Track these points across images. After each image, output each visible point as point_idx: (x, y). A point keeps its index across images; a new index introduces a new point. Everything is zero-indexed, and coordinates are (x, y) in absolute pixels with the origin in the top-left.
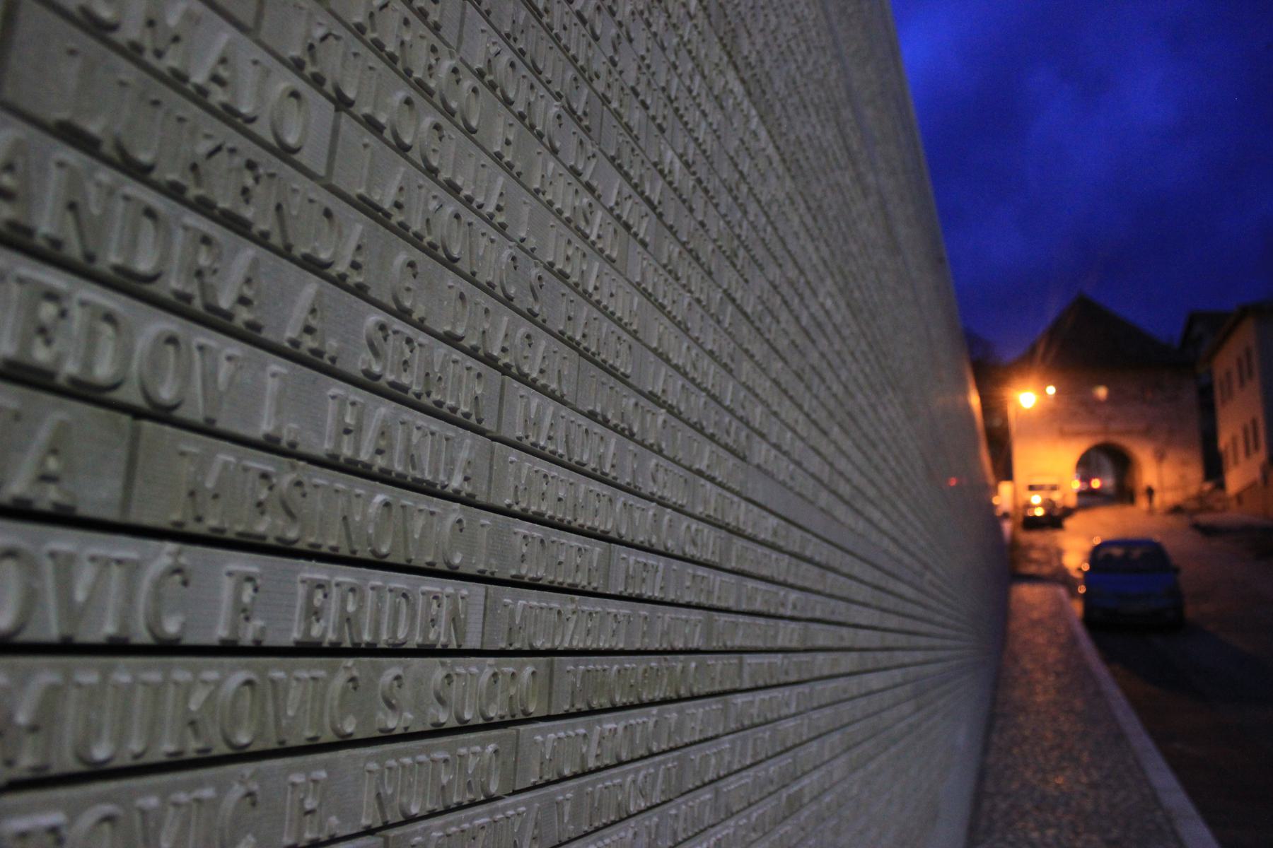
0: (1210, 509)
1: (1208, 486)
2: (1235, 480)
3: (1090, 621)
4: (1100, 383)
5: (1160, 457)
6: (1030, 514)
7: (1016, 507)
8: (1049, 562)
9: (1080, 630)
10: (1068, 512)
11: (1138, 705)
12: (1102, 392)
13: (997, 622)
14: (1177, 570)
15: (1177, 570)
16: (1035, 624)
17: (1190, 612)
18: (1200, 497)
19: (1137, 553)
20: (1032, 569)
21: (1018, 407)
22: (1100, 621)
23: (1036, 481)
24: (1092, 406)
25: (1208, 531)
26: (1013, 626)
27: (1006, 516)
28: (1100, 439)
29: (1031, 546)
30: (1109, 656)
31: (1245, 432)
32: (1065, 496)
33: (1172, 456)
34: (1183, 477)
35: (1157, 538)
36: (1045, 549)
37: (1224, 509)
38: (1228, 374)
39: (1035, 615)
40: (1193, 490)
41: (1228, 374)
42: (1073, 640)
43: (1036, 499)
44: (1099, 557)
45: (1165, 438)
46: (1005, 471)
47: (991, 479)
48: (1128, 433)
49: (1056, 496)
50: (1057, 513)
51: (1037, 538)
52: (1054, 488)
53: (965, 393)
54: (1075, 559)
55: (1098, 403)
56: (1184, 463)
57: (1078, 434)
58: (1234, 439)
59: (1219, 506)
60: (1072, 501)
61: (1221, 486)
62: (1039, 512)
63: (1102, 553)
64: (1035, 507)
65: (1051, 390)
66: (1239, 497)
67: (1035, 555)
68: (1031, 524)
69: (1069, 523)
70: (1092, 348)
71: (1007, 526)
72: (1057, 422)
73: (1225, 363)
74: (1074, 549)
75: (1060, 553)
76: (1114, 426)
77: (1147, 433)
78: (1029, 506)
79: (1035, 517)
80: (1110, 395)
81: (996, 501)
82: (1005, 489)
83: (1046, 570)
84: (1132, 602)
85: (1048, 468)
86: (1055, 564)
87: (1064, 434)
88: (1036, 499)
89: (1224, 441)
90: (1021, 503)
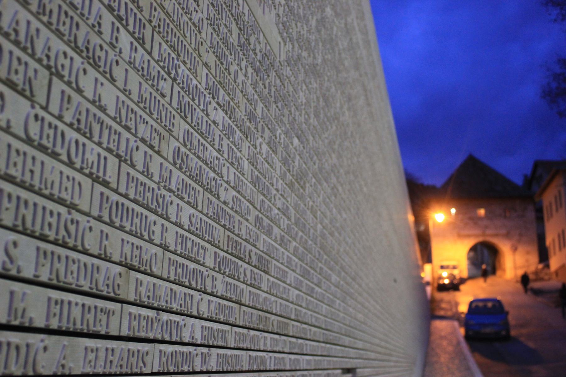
0: (542, 279)
1: (540, 266)
2: (555, 263)
3: (468, 338)
4: (481, 207)
5: (515, 249)
6: (441, 282)
7: (433, 278)
8: (451, 310)
9: (462, 340)
10: (463, 281)
11: (480, 366)
12: (482, 212)
13: (427, 339)
14: (507, 313)
15: (507, 313)
16: (442, 338)
17: (513, 333)
18: (536, 273)
19: (490, 305)
20: (442, 313)
21: (435, 224)
22: (474, 338)
23: (445, 263)
24: (475, 220)
25: (537, 292)
26: (432, 338)
27: (428, 283)
28: (480, 239)
29: (441, 301)
30: (473, 349)
31: (559, 236)
32: (461, 272)
33: (521, 249)
34: (527, 261)
35: (499, 298)
36: (449, 302)
37: (549, 279)
38: (551, 204)
39: (443, 334)
40: (532, 269)
41: (551, 204)
42: (458, 343)
43: (445, 274)
44: (474, 308)
45: (517, 237)
46: (427, 257)
47: (420, 262)
48: (497, 235)
49: (456, 272)
50: (456, 282)
51: (445, 296)
52: (454, 267)
53: (406, 213)
54: (463, 308)
55: (480, 218)
56: (528, 253)
57: (468, 236)
58: (554, 241)
59: (546, 277)
60: (465, 274)
61: (548, 266)
62: (447, 281)
63: (474, 305)
64: (444, 278)
65: (453, 211)
66: (557, 273)
67: (444, 305)
68: (442, 288)
69: (462, 287)
70: (475, 185)
71: (429, 289)
72: (456, 230)
73: (548, 198)
74: (463, 301)
75: (457, 304)
76: (488, 232)
77: (507, 236)
78: (440, 278)
79: (444, 284)
80: (486, 213)
81: (423, 275)
82: (428, 268)
83: (449, 313)
84: (486, 328)
85: (452, 255)
86: (454, 310)
87: (461, 236)
88: (445, 274)
89: (549, 241)
90: (436, 276)
